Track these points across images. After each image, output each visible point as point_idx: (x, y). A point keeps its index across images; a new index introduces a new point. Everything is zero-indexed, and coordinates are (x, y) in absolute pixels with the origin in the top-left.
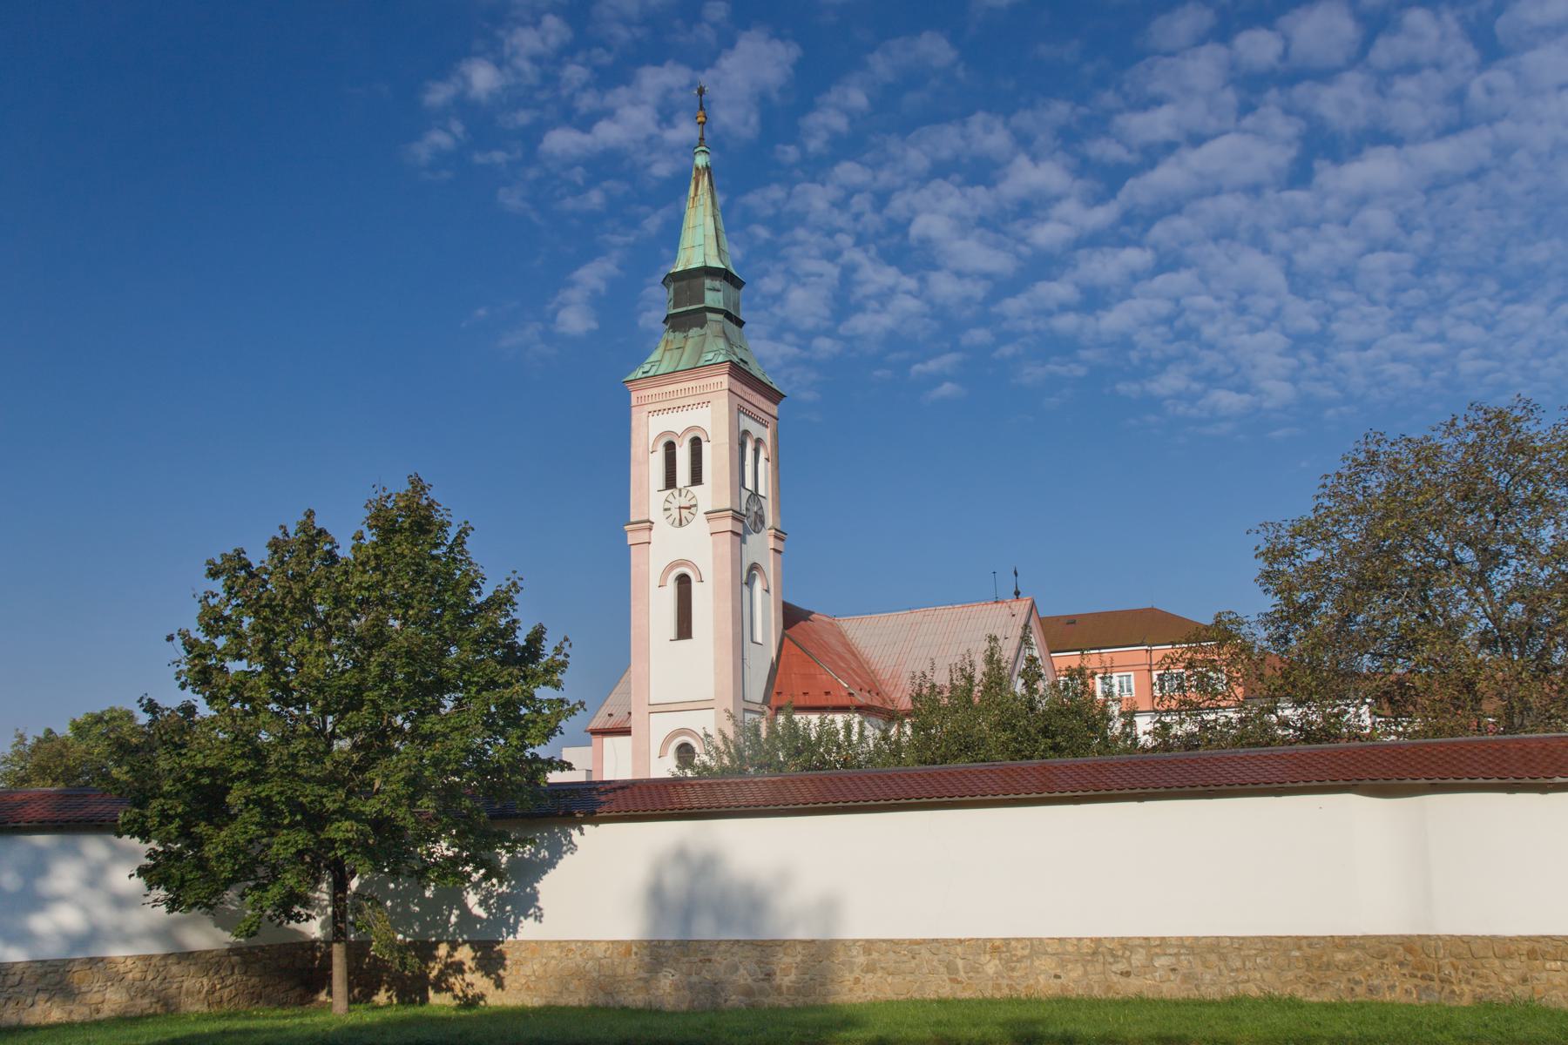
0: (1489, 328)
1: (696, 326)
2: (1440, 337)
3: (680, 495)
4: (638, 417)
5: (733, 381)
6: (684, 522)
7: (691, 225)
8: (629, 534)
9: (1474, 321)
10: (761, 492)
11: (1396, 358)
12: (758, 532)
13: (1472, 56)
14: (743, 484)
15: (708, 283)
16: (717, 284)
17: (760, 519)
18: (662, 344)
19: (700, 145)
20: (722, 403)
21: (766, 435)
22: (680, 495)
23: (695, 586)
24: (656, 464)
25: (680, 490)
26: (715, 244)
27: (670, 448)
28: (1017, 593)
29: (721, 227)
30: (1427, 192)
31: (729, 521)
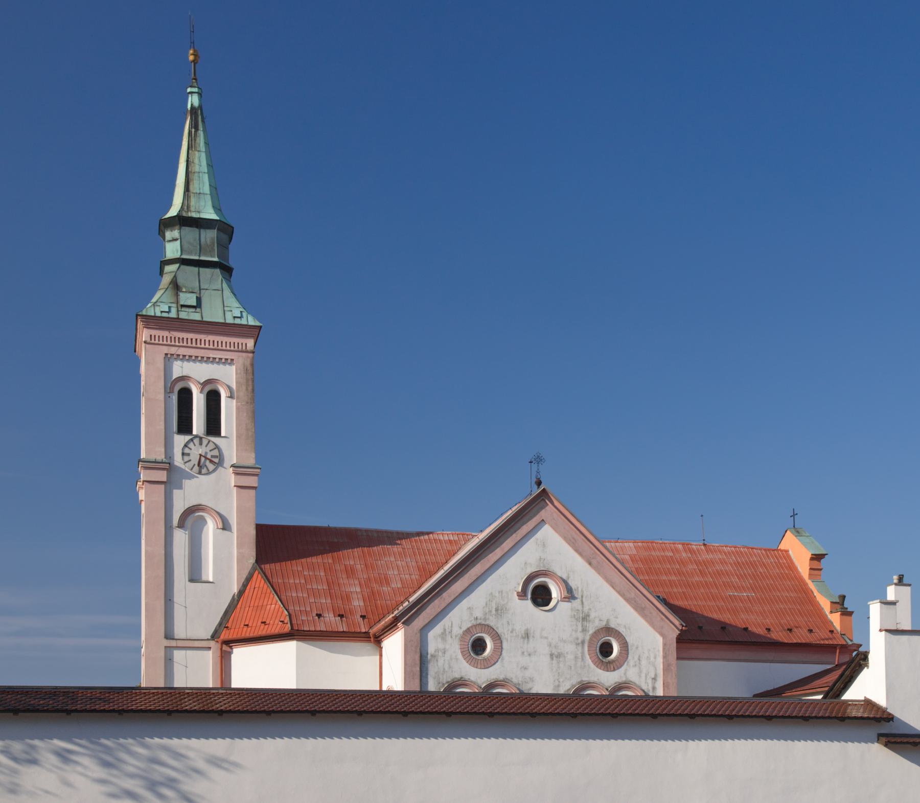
14: (185, 426)
16: (176, 233)
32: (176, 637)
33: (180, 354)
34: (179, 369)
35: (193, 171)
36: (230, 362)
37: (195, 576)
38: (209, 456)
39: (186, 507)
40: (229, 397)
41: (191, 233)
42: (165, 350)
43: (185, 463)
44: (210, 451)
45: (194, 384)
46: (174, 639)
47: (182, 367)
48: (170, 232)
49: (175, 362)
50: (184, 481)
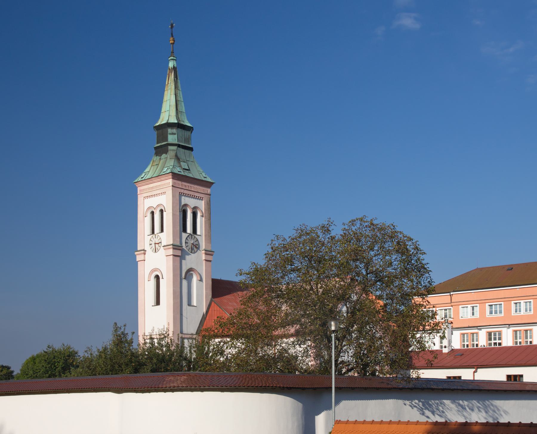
1: (164, 153)
4: (140, 199)
5: (175, 181)
6: (157, 250)
7: (165, 100)
8: (137, 256)
10: (198, 232)
12: (194, 253)
14: (184, 230)
15: (170, 130)
16: (174, 131)
17: (196, 247)
18: (151, 162)
19: (171, 56)
20: (169, 191)
21: (202, 205)
22: (155, 238)
23: (161, 280)
24: (148, 219)
25: (155, 235)
26: (174, 110)
27: (153, 213)
29: (181, 98)
31: (171, 250)
32: (183, 333)
33: (185, 193)
34: (185, 200)
35: (178, 100)
36: (201, 199)
37: (189, 304)
38: (195, 244)
39: (187, 269)
40: (202, 216)
41: (181, 131)
42: (180, 190)
43: (186, 247)
44: (195, 242)
45: (189, 208)
46: (183, 334)
47: (185, 200)
48: (171, 130)
49: (182, 197)
50: (186, 256)
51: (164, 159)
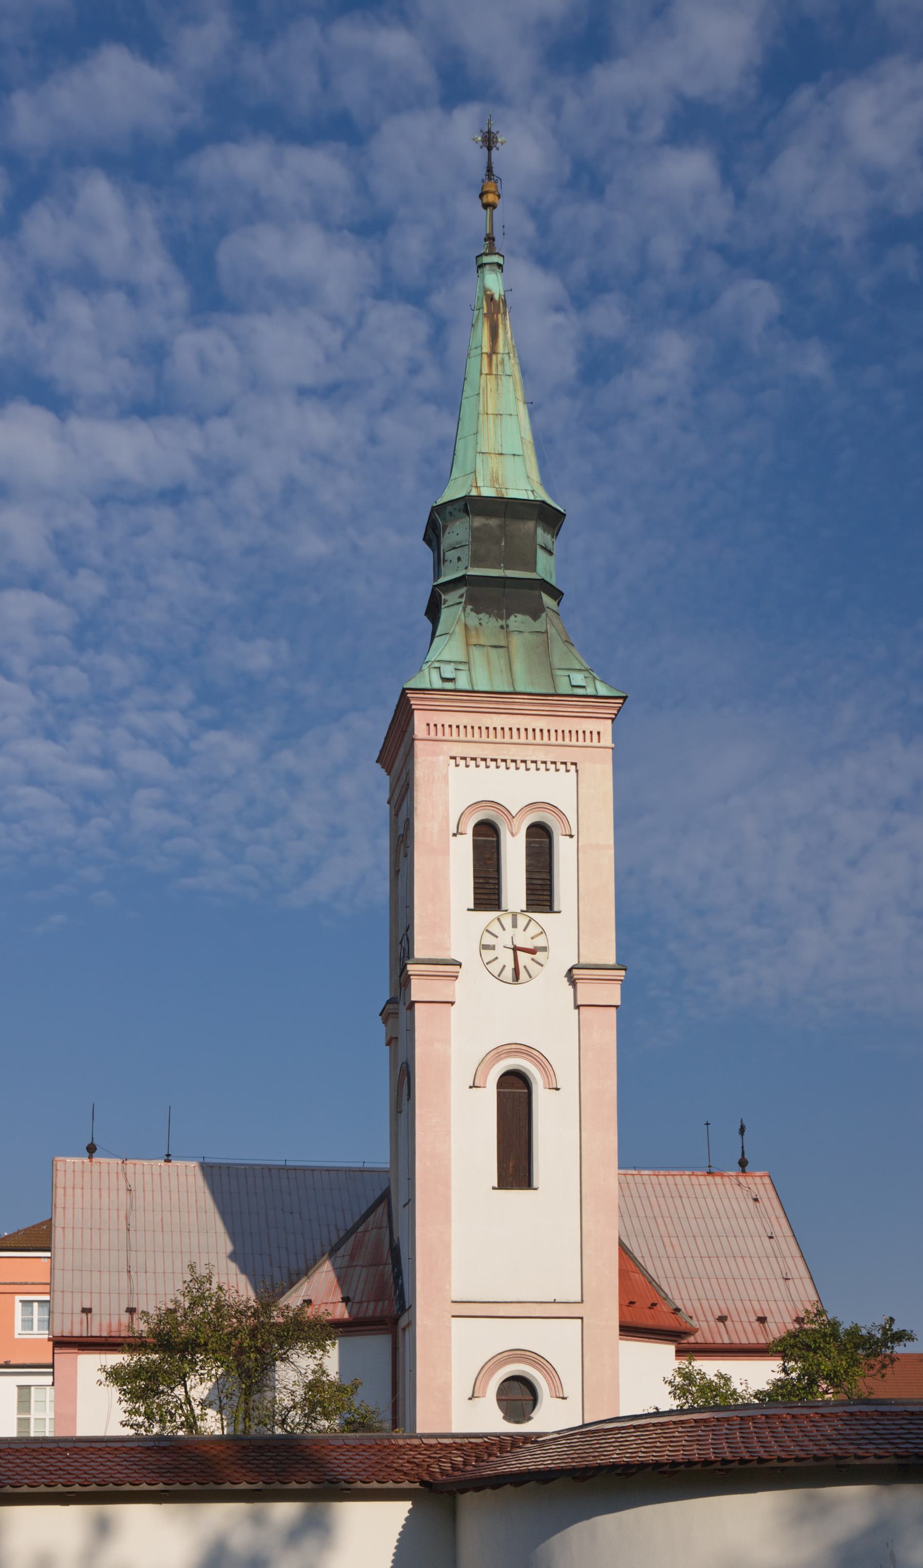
0: (178, 761)
1: (524, 612)
2: (106, 762)
3: (515, 925)
6: (523, 974)
9: (153, 744)
11: (32, 779)
13: (180, 296)
22: (515, 925)
25: (514, 915)
28: (743, 1163)
30: (101, 502)
51: (526, 634)
